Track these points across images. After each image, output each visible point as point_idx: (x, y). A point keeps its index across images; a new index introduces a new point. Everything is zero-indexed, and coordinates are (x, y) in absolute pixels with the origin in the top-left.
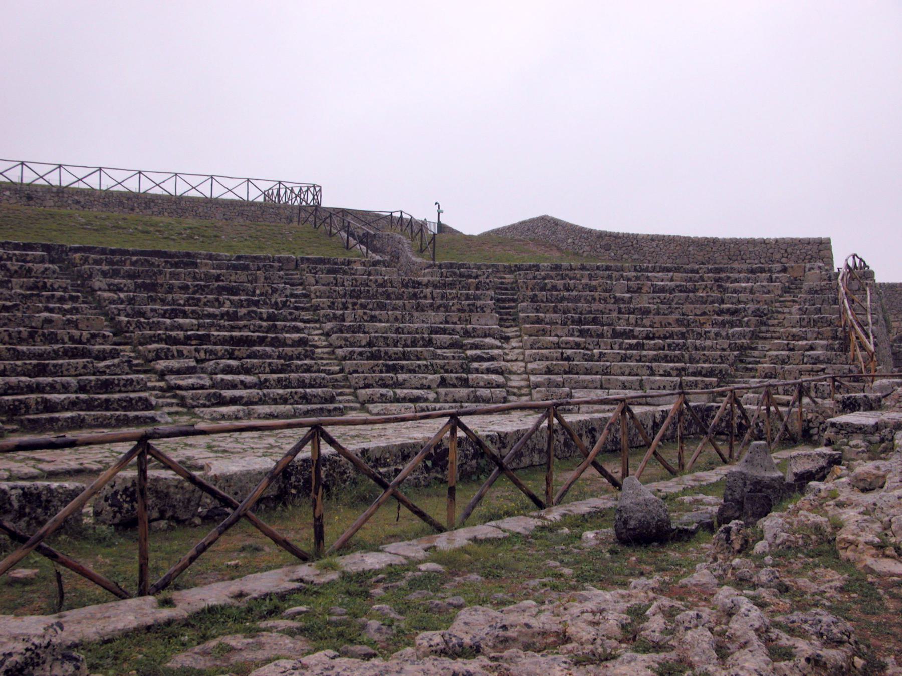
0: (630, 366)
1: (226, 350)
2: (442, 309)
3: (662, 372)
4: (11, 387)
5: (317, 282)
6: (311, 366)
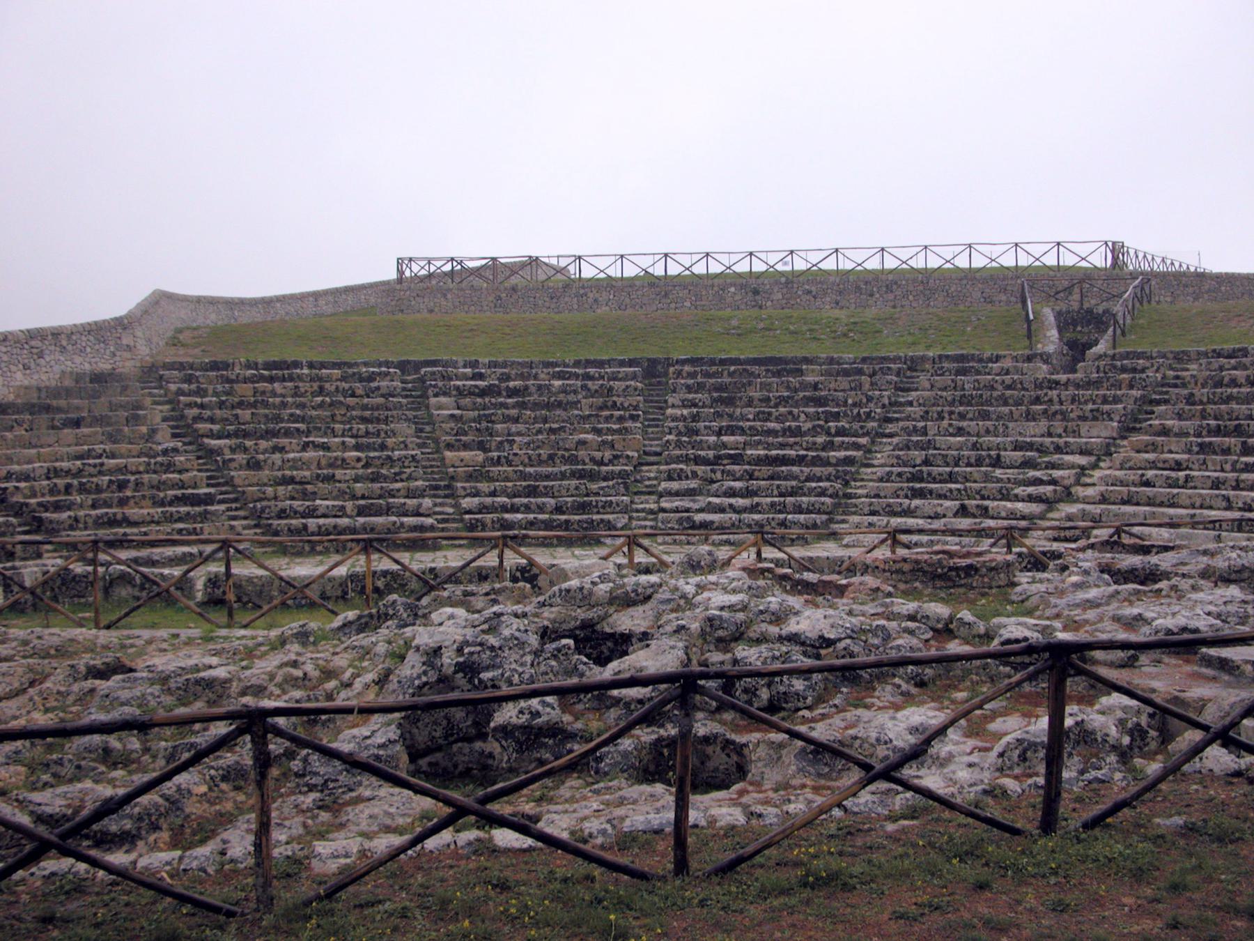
0: (1200, 495)
1: (746, 471)
2: (1059, 417)
3: (1240, 505)
4: (485, 507)
5: (932, 386)
6: (826, 489)
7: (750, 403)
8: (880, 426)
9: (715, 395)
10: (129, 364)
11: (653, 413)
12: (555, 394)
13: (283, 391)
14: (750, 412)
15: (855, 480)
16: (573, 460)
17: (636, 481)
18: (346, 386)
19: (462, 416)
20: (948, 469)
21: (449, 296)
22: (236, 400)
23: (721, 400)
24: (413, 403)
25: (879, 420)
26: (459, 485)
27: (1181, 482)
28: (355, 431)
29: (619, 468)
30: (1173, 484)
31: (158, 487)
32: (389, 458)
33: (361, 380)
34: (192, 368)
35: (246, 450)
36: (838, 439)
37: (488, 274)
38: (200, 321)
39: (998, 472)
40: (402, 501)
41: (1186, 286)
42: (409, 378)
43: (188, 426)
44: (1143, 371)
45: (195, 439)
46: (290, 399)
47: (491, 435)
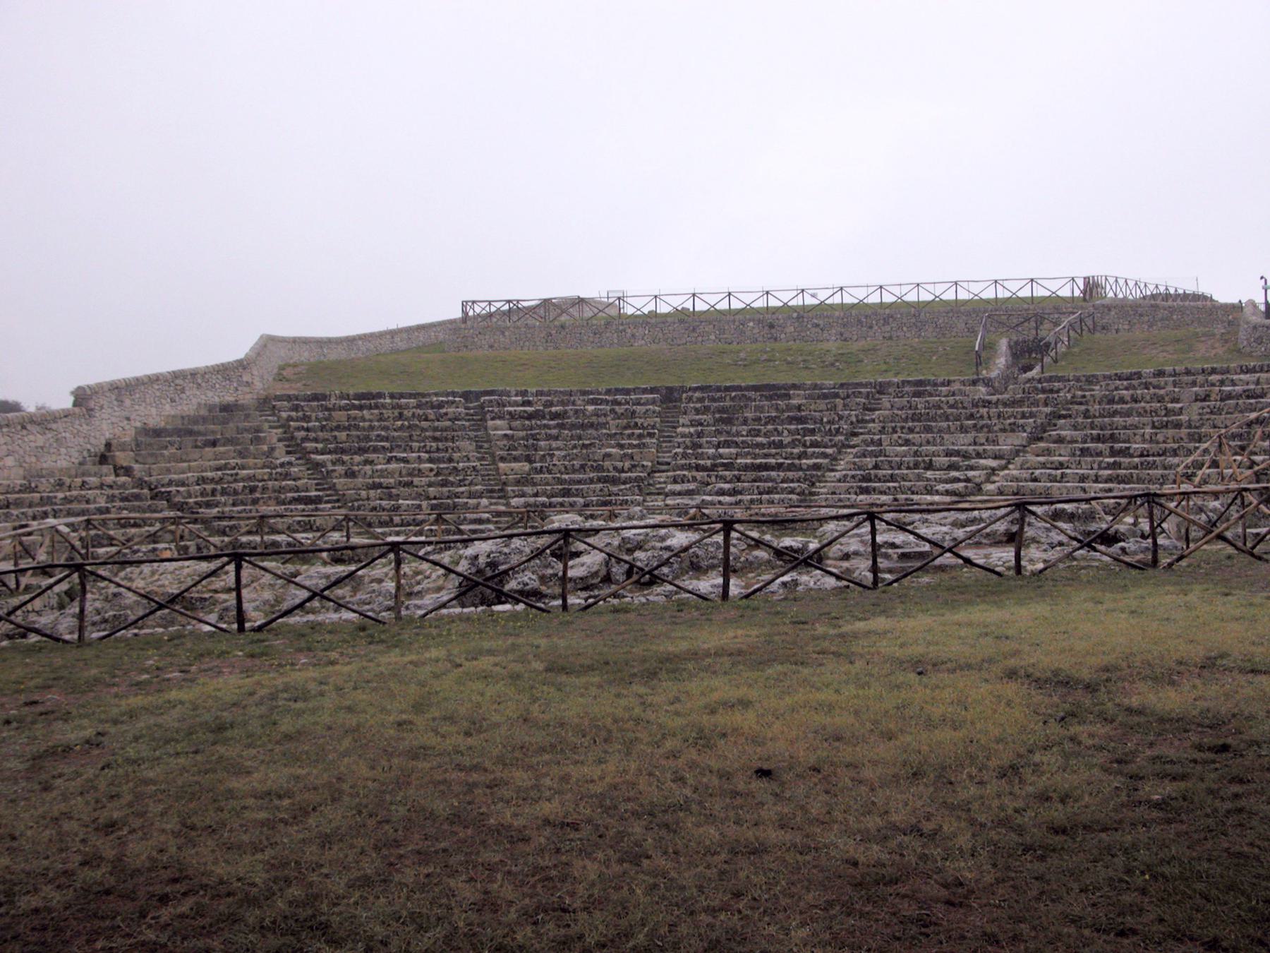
0: (1066, 487)
1: (734, 476)
2: (985, 430)
6: (795, 489)
7: (745, 422)
8: (846, 439)
9: (717, 416)
10: (249, 396)
11: (668, 431)
12: (589, 417)
13: (371, 417)
14: (744, 429)
15: (820, 482)
16: (599, 469)
17: (649, 485)
18: (420, 412)
19: (513, 436)
20: (890, 472)
21: (507, 333)
22: (334, 424)
23: (722, 420)
24: (473, 425)
25: (846, 435)
26: (509, 488)
27: (1058, 478)
28: (428, 448)
29: (635, 474)
30: (1053, 479)
31: (281, 490)
32: (455, 468)
33: (432, 407)
34: (297, 399)
35: (344, 463)
36: (810, 450)
37: (542, 312)
38: (296, 358)
39: (929, 474)
40: (465, 500)
41: (1141, 315)
42: (471, 405)
43: (298, 445)
44: (1058, 391)
45: (304, 455)
46: (376, 423)
47: (536, 450)
